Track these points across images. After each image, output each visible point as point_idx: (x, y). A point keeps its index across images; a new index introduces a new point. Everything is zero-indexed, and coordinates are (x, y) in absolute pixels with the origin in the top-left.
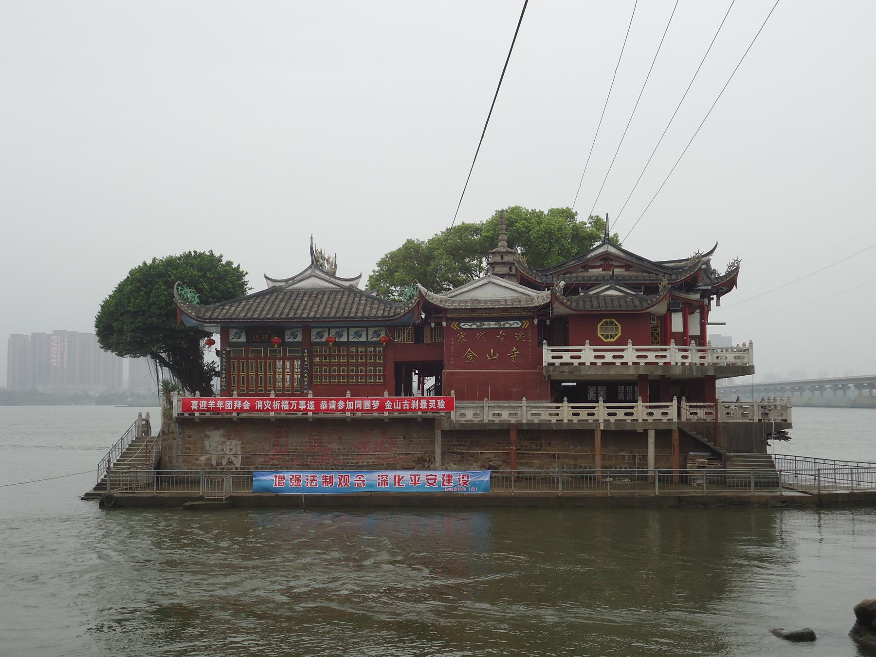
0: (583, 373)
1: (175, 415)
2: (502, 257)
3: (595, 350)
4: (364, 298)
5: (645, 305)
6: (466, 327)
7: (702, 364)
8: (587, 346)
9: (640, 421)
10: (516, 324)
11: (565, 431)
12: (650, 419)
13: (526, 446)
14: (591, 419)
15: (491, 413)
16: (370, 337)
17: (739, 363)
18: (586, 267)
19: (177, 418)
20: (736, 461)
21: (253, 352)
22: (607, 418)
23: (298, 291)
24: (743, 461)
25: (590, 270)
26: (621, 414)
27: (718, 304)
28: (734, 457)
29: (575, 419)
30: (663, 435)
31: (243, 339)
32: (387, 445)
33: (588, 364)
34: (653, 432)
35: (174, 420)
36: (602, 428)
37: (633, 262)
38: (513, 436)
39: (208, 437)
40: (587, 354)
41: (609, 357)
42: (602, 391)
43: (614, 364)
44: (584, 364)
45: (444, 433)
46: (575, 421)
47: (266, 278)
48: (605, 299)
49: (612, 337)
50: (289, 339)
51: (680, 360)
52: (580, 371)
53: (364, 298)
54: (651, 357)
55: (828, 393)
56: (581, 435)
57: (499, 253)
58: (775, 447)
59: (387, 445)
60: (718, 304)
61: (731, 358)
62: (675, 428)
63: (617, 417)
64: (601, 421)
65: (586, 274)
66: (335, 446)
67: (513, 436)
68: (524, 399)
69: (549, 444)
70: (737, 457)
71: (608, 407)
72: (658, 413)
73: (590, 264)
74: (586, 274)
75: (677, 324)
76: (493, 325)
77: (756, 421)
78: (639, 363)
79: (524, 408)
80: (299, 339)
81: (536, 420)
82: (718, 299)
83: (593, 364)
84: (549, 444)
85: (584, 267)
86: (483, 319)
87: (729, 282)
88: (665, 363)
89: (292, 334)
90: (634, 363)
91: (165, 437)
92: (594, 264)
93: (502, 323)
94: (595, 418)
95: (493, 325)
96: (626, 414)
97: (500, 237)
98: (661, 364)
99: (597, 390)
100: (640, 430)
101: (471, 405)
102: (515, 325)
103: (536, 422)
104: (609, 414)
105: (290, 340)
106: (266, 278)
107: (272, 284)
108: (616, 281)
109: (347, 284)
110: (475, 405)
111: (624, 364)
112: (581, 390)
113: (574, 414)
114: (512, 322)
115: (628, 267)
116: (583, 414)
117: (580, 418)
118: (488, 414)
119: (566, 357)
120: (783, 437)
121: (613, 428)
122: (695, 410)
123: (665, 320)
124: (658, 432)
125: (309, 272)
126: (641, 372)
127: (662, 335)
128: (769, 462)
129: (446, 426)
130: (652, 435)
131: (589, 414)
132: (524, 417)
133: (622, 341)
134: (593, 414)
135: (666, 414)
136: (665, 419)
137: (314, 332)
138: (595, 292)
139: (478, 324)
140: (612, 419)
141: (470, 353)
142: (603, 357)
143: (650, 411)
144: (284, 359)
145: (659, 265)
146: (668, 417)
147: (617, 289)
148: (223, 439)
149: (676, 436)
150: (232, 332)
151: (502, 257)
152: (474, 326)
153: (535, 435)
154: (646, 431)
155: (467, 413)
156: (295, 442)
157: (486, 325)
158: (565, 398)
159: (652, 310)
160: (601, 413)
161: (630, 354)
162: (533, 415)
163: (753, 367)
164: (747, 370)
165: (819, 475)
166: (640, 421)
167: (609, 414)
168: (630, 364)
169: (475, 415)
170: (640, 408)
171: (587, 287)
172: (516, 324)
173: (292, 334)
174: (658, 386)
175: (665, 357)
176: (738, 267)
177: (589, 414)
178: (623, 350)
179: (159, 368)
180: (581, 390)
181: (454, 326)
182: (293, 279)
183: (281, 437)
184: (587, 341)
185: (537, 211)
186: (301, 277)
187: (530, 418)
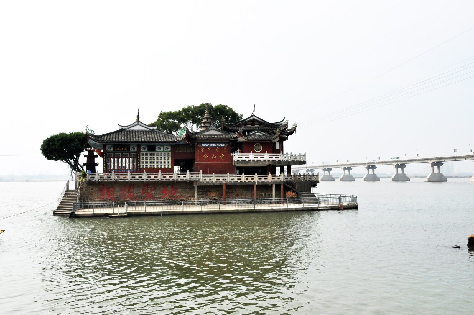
4: (137, 133)
10: (223, 145)
11: (244, 185)
12: (273, 180)
14: (266, 181)
23: (132, 131)
29: (247, 181)
30: (278, 186)
31: (112, 149)
40: (251, 156)
41: (259, 158)
45: (198, 187)
53: (137, 133)
54: (274, 158)
55: (160, 166)
58: (313, 190)
61: (298, 159)
66: (153, 192)
75: (278, 146)
76: (214, 145)
80: (135, 150)
81: (233, 181)
86: (210, 143)
88: (273, 160)
95: (214, 145)
111: (265, 160)
112: (250, 170)
116: (250, 179)
120: (315, 186)
122: (134, 176)
124: (276, 185)
125: (137, 123)
128: (313, 195)
130: (274, 186)
140: (260, 181)
141: (205, 156)
144: (114, 157)
145: (272, 124)
149: (224, 187)
150: (107, 147)
154: (272, 185)
156: (137, 192)
157: (212, 145)
160: (256, 178)
161: (267, 156)
164: (304, 163)
167: (133, 177)
172: (223, 145)
176: (288, 123)
180: (250, 170)
181: (199, 145)
186: (133, 125)
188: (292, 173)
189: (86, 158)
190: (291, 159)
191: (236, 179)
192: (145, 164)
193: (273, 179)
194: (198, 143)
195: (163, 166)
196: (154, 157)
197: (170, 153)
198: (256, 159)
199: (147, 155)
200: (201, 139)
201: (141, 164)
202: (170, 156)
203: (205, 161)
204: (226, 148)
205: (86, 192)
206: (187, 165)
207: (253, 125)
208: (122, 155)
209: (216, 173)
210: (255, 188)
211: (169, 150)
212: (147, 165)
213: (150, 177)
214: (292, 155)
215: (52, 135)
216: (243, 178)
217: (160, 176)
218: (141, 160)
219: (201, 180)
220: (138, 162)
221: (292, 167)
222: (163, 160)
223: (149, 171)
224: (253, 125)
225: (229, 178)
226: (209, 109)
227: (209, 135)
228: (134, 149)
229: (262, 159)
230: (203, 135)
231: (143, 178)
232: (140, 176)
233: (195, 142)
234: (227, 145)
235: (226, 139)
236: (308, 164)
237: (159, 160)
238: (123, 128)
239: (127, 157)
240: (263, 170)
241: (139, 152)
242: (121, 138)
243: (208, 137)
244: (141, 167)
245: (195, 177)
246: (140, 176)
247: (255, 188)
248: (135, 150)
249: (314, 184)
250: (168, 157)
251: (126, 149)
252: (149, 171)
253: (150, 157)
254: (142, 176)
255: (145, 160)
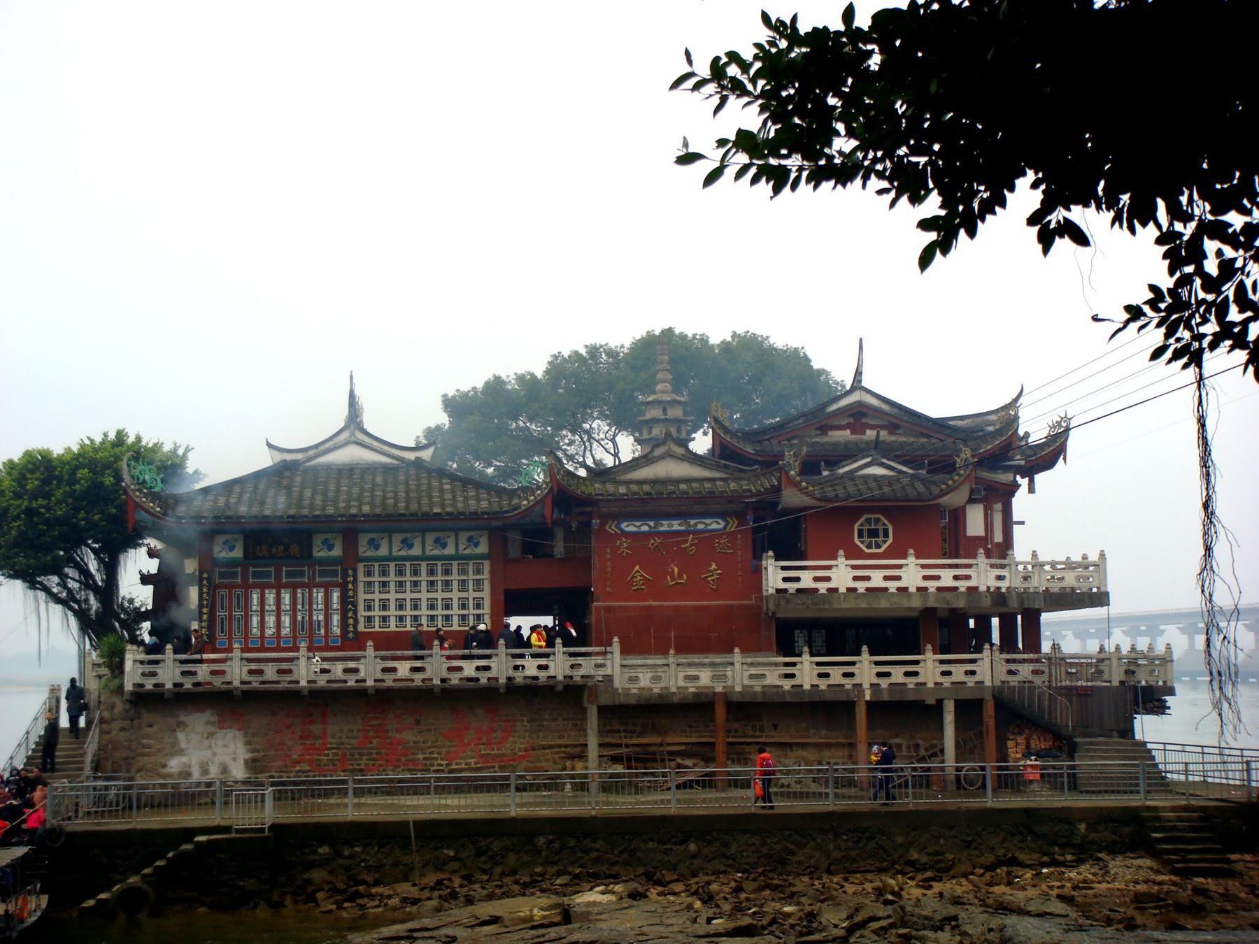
0: (836, 606)
1: (128, 687)
2: (665, 411)
3: (854, 567)
5: (935, 490)
6: (632, 529)
7: (998, 588)
8: (911, 560)
9: (931, 685)
10: (716, 525)
13: (736, 731)
15: (681, 675)
16: (461, 547)
17: (1081, 588)
18: (823, 429)
19: (133, 693)
20: (1088, 750)
21: (289, 574)
22: (876, 680)
24: (1117, 751)
25: (830, 433)
26: (897, 674)
27: (1031, 490)
28: (1085, 744)
29: (823, 684)
30: (969, 709)
31: (238, 553)
32: (499, 734)
33: (842, 590)
34: (952, 703)
35: (126, 697)
36: (868, 698)
37: (902, 419)
38: (720, 713)
39: (181, 725)
40: (842, 575)
41: (877, 579)
42: (819, 638)
43: (886, 589)
44: (836, 590)
45: (604, 711)
46: (947, 685)
47: (270, 445)
48: (866, 483)
49: (878, 546)
50: (319, 553)
51: (993, 584)
52: (830, 603)
54: (947, 578)
56: (830, 711)
57: (660, 402)
58: (1147, 727)
59: (499, 734)
60: (1031, 490)
61: (1070, 580)
62: (988, 696)
63: (893, 680)
64: (866, 686)
65: (825, 439)
66: (409, 736)
67: (720, 713)
68: (737, 650)
69: (775, 726)
70: (1091, 744)
71: (877, 663)
72: (958, 672)
73: (830, 422)
74: (825, 439)
75: (975, 523)
76: (676, 526)
77: (1116, 683)
78: (855, 589)
79: (738, 666)
80: (337, 552)
81: (757, 686)
82: (1032, 482)
83: (851, 590)
84: (775, 726)
85: (819, 428)
87: (1051, 452)
88: (969, 589)
89: (437, 541)
90: (919, 589)
91: (104, 726)
92: (837, 423)
93: (692, 522)
94: (856, 680)
95: (676, 526)
96: (907, 674)
97: (659, 376)
98: (823, 591)
99: (810, 636)
100: (931, 701)
101: (639, 662)
102: (714, 526)
103: (758, 689)
104: (879, 675)
105: (322, 554)
106: (270, 445)
107: (279, 457)
108: (880, 450)
109: (411, 456)
110: (649, 662)
112: (840, 632)
113: (821, 675)
114: (708, 521)
115: (893, 428)
116: (836, 675)
117: (832, 681)
118: (677, 678)
119: (807, 580)
120: (1158, 707)
121: (886, 698)
123: (958, 516)
124: (961, 706)
125: (345, 435)
126: (931, 603)
127: (954, 543)
129: (604, 700)
130: (949, 707)
131: (845, 675)
132: (738, 680)
133: (898, 551)
134: (916, 674)
135: (973, 673)
136: (970, 681)
137: (363, 540)
138: (847, 469)
139: (652, 524)
140: (884, 683)
142: (868, 578)
143: (946, 668)
145: (941, 425)
146: (977, 678)
147: (882, 465)
148: (211, 729)
149: (989, 710)
151: (665, 411)
152: (645, 528)
153: (751, 711)
154: (940, 703)
155: (640, 675)
157: (665, 526)
158: (865, 648)
159: (945, 500)
160: (865, 672)
161: (912, 573)
162: (752, 677)
163: (1107, 593)
164: (1100, 599)
165: (1248, 770)
166: (931, 685)
167: (879, 675)
168: (912, 590)
169: (656, 679)
170: (930, 664)
171: (833, 463)
173: (325, 542)
174: (951, 627)
175: (968, 577)
177: (845, 675)
178: (899, 567)
179: (43, 606)
181: (611, 528)
182: (316, 446)
183: (313, 722)
184: (911, 551)
185: (677, 331)
187: (747, 682)
188: (1046, 647)
189: (150, 588)
190: (1039, 583)
191: (773, 678)
192: (377, 613)
193: (944, 673)
194: (605, 518)
195: (393, 622)
196: (447, 583)
197: (487, 565)
198: (861, 586)
199: (416, 572)
200: (620, 499)
201: (362, 613)
202: (486, 575)
203: (639, 594)
204: (731, 535)
205: (124, 736)
206: (576, 617)
207: (857, 428)
208: (278, 576)
209: (680, 650)
210: (861, 714)
211: (483, 548)
212: (384, 619)
213: (394, 670)
214: (1038, 565)
215: (780, 339)
216: (807, 671)
217: (437, 667)
218: (362, 597)
219: (617, 684)
220: (348, 604)
221: (1045, 617)
222: (424, 595)
223: (390, 643)
224: (857, 428)
225: (745, 673)
226: (673, 362)
227: (654, 482)
228: (331, 548)
229: (892, 586)
230: (628, 483)
231: (362, 675)
232: (352, 665)
233: (590, 514)
234: (733, 525)
235: (732, 499)
236: (1117, 606)
237: (408, 596)
238: (289, 457)
239: (302, 585)
240: (895, 632)
241: (350, 561)
242: (277, 505)
243: (646, 488)
244: (361, 628)
245: (587, 667)
246: (352, 665)
247: (861, 714)
248: (337, 552)
249: (1153, 700)
250: (478, 583)
251: (295, 549)
252: (390, 643)
253: (400, 584)
254: (493, 663)
255: (376, 596)
